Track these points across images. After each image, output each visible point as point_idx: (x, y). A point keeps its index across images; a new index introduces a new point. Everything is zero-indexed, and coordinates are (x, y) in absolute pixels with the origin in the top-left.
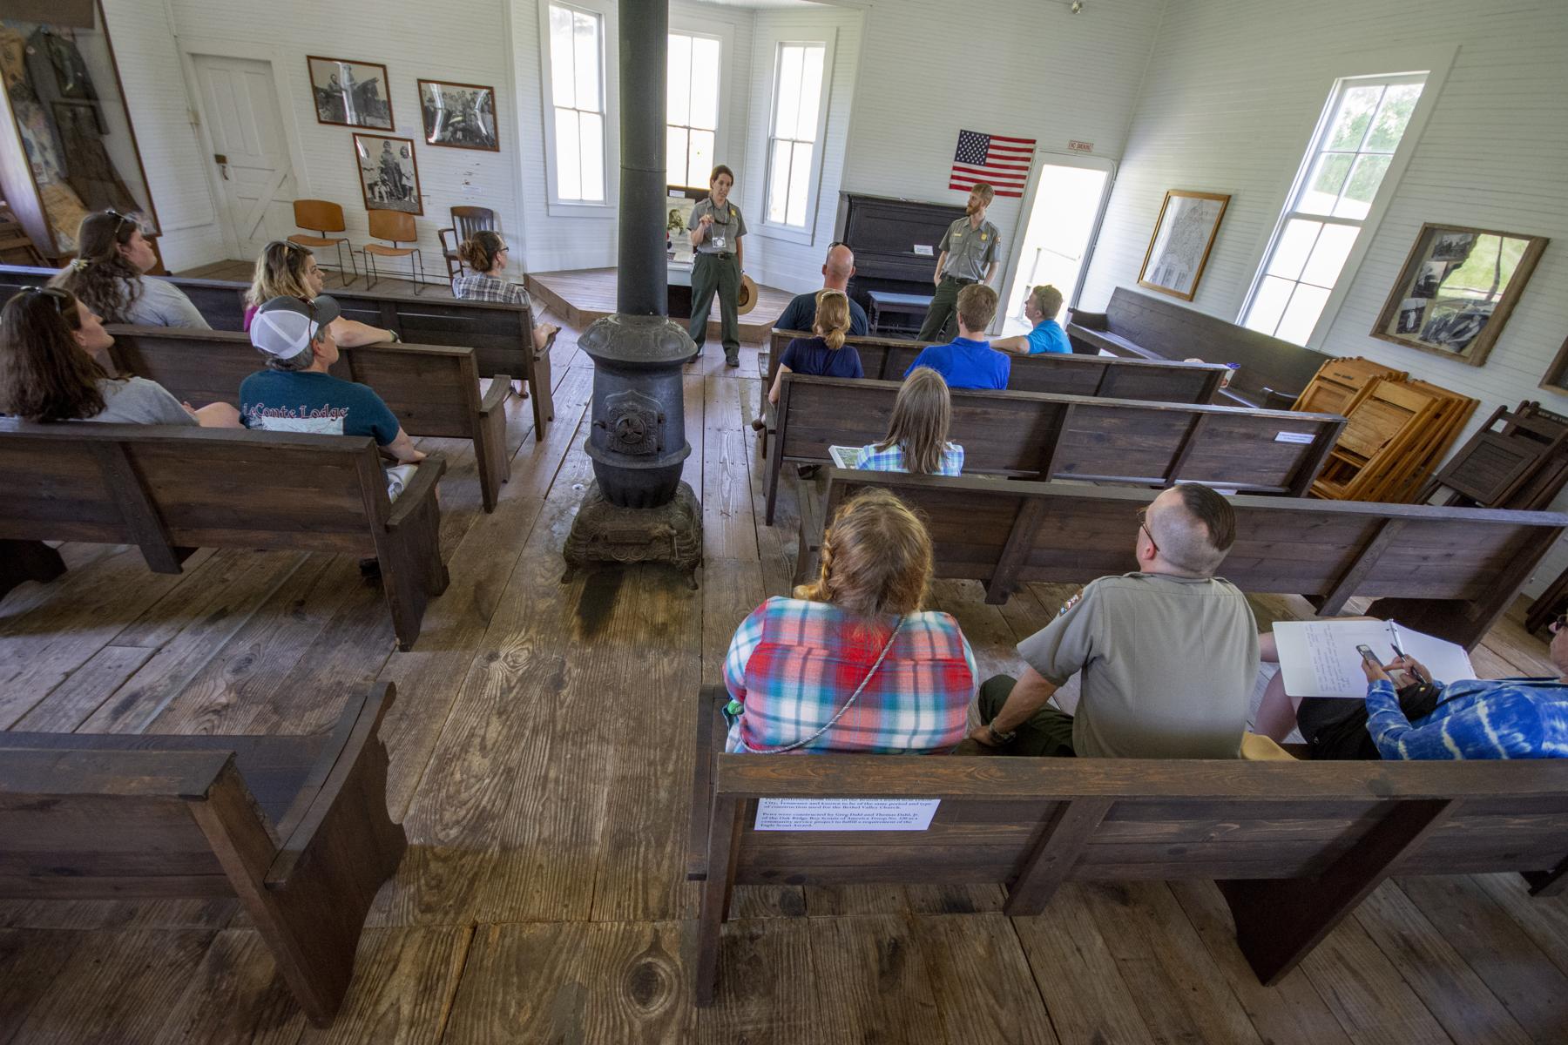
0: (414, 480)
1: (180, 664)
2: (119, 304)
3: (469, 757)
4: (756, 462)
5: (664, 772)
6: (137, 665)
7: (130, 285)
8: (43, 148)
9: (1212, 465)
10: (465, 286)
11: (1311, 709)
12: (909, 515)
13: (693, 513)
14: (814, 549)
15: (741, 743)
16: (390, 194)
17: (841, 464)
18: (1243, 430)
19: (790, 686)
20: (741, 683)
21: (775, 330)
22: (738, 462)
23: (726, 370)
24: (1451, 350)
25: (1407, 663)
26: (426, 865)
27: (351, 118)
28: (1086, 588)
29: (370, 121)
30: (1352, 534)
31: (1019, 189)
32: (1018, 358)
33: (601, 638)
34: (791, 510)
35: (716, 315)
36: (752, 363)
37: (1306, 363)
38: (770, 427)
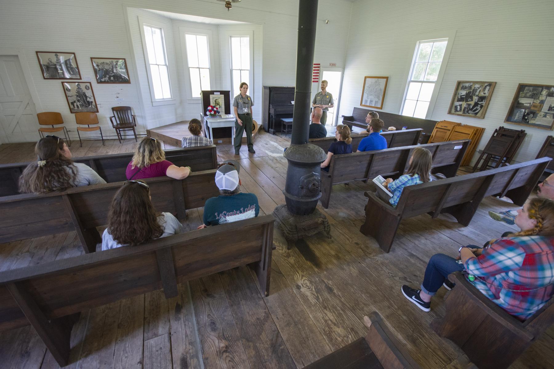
1: (187, 336)
2: (70, 178)
7: (71, 168)
16: (82, 105)
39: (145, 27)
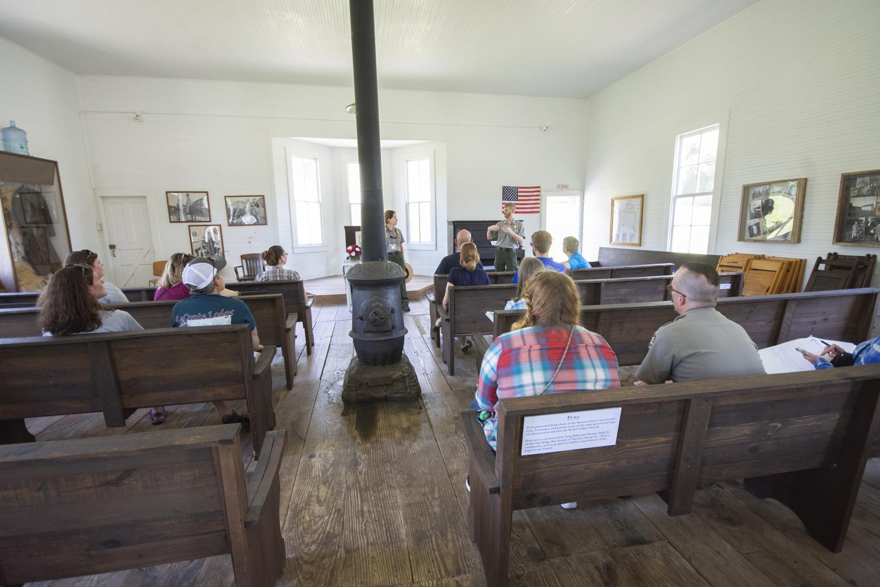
5: (433, 498)
8: (17, 244)
26: (301, 568)
27: (183, 219)
33: (373, 439)
39: (293, 158)
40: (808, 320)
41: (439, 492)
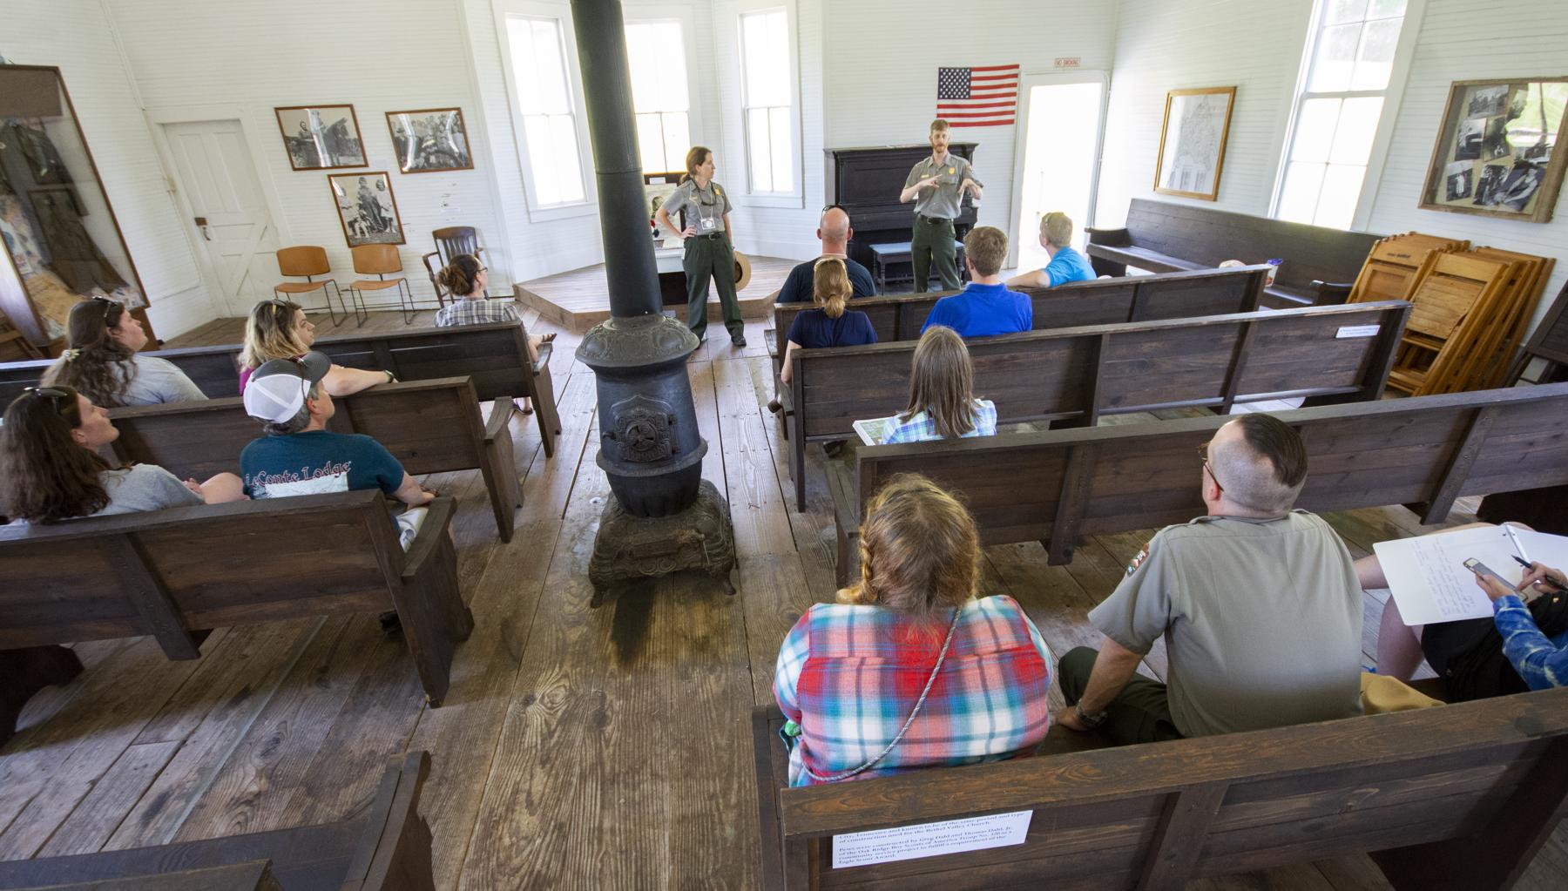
0: (426, 523)
1: (207, 754)
2: (115, 388)
3: (516, 816)
4: (779, 445)
5: (727, 806)
6: (163, 761)
7: (124, 367)
8: (24, 239)
9: (1274, 373)
10: (451, 313)
11: (1437, 638)
12: (946, 497)
13: (720, 512)
14: (852, 535)
15: (805, 770)
16: (371, 228)
17: (869, 442)
18: (1299, 333)
19: (847, 702)
20: (795, 704)
21: (778, 305)
22: (759, 448)
23: (733, 351)
24: (1511, 209)
25: (1538, 573)
27: (324, 160)
28: (1151, 543)
29: (343, 160)
30: (1439, 433)
31: (1005, 114)
32: (1038, 293)
33: (639, 664)
34: (822, 490)
35: (714, 296)
36: (759, 338)
37: (1355, 247)
38: (788, 408)
40: (1520, 439)
41: (739, 791)
